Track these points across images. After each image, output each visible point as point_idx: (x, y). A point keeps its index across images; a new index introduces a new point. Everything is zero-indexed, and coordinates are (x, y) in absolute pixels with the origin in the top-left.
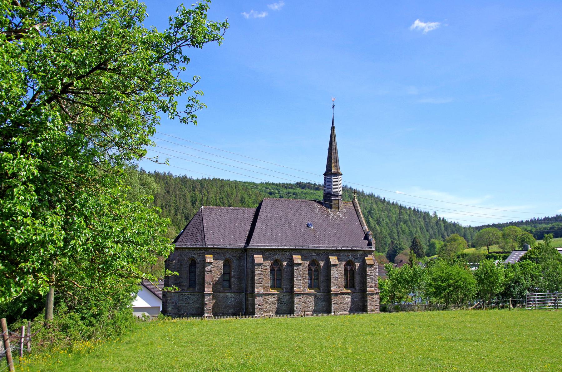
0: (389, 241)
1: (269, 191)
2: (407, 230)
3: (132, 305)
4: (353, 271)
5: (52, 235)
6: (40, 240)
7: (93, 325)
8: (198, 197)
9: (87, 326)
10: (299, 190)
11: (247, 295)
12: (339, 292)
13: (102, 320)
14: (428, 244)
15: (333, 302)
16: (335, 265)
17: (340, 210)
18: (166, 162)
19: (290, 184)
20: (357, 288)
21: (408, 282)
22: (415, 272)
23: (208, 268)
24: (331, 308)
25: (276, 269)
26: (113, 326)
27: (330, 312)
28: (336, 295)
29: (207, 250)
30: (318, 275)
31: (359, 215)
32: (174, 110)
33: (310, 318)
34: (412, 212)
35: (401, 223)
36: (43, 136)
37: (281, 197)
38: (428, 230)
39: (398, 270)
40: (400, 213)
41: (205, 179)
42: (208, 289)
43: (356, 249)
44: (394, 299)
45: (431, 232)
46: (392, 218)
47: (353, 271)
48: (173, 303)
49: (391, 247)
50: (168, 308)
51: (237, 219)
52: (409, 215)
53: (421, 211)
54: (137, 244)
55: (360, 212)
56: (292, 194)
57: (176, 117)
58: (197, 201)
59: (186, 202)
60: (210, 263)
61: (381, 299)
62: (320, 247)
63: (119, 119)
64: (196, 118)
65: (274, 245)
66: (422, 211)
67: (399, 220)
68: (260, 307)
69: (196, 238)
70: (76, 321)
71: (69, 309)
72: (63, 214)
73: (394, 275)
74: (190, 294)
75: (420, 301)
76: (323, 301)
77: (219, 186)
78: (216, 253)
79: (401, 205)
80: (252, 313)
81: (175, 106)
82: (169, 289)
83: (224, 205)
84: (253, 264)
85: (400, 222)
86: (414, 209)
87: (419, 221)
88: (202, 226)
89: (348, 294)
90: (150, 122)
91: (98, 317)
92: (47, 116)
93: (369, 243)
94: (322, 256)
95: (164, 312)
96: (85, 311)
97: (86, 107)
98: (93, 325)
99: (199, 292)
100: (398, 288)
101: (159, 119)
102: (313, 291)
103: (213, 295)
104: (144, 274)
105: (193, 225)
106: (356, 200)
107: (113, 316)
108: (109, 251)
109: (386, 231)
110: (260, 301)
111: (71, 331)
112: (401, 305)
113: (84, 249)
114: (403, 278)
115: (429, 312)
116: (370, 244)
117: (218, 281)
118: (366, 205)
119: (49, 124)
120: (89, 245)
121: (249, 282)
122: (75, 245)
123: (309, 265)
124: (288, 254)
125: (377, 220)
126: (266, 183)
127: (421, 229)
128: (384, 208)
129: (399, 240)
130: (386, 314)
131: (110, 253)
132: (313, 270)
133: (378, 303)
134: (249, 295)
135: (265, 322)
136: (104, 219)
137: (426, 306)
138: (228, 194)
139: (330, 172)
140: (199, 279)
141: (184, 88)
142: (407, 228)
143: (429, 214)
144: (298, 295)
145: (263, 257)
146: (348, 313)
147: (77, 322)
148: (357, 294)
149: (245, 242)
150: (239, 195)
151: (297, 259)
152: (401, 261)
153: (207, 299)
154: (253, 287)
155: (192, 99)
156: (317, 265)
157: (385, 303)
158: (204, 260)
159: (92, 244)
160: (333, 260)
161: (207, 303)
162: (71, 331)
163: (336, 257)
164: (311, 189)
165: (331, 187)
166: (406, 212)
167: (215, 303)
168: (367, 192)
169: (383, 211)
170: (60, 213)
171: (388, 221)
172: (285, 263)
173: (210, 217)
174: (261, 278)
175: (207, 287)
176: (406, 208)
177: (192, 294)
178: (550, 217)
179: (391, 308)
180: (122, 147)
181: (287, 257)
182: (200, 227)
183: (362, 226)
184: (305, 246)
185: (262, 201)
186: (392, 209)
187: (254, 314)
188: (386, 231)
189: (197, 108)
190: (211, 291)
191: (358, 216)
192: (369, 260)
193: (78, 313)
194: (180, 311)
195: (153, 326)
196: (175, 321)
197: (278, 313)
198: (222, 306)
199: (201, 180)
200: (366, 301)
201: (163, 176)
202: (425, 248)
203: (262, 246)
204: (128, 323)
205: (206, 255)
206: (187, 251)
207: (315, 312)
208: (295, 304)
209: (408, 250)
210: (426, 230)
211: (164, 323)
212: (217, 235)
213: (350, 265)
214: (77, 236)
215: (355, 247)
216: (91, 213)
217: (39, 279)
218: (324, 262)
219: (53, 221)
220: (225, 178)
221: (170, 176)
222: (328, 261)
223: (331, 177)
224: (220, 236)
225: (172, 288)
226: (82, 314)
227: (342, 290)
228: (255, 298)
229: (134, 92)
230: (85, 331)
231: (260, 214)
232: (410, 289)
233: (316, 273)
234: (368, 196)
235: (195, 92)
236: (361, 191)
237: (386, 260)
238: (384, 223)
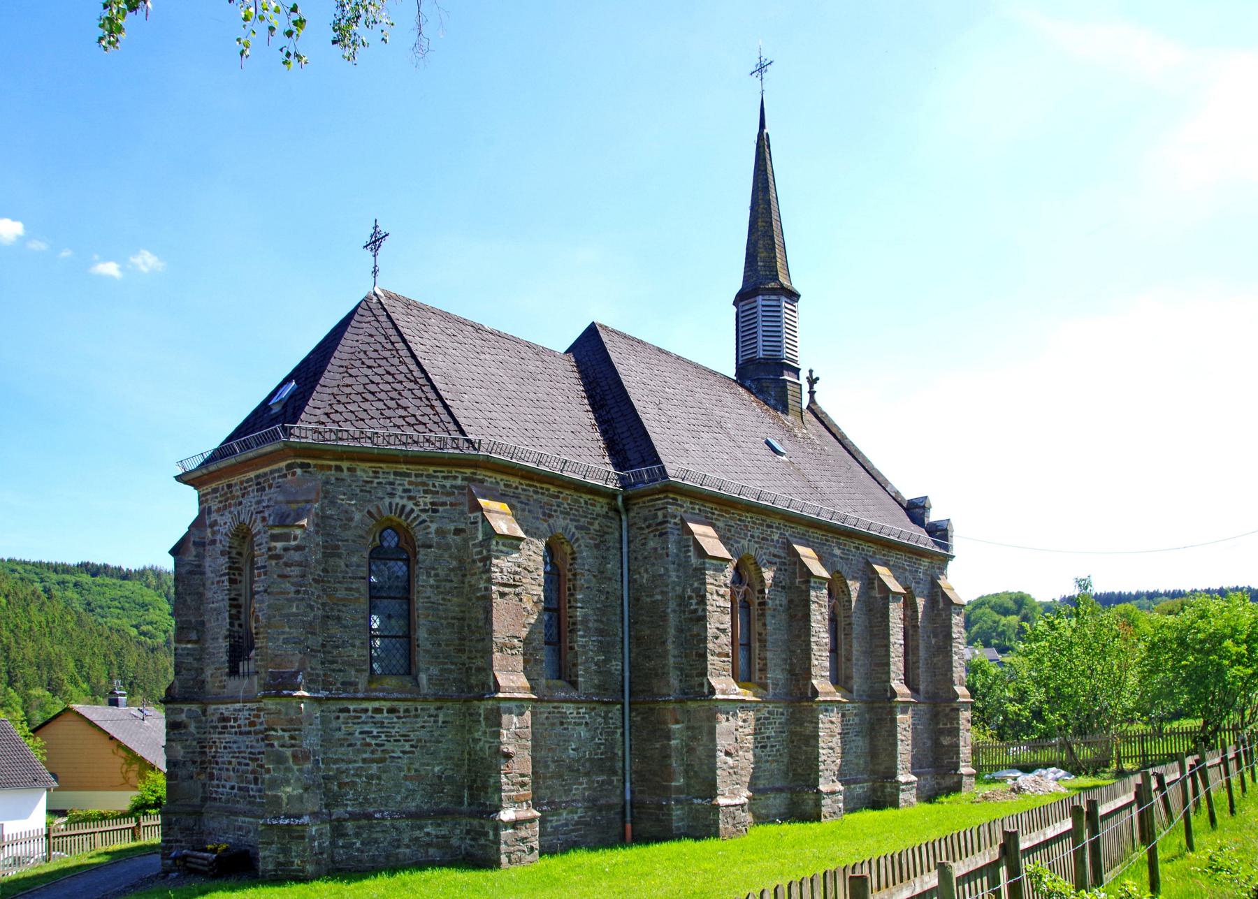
10: (86, 578)
19: (64, 565)
74: (392, 711)
126: (9, 560)
140: (433, 631)
161: (511, 749)
164: (112, 576)
172: (768, 575)
175: (504, 669)
177: (402, 706)
178: (18, 559)
206: (364, 471)
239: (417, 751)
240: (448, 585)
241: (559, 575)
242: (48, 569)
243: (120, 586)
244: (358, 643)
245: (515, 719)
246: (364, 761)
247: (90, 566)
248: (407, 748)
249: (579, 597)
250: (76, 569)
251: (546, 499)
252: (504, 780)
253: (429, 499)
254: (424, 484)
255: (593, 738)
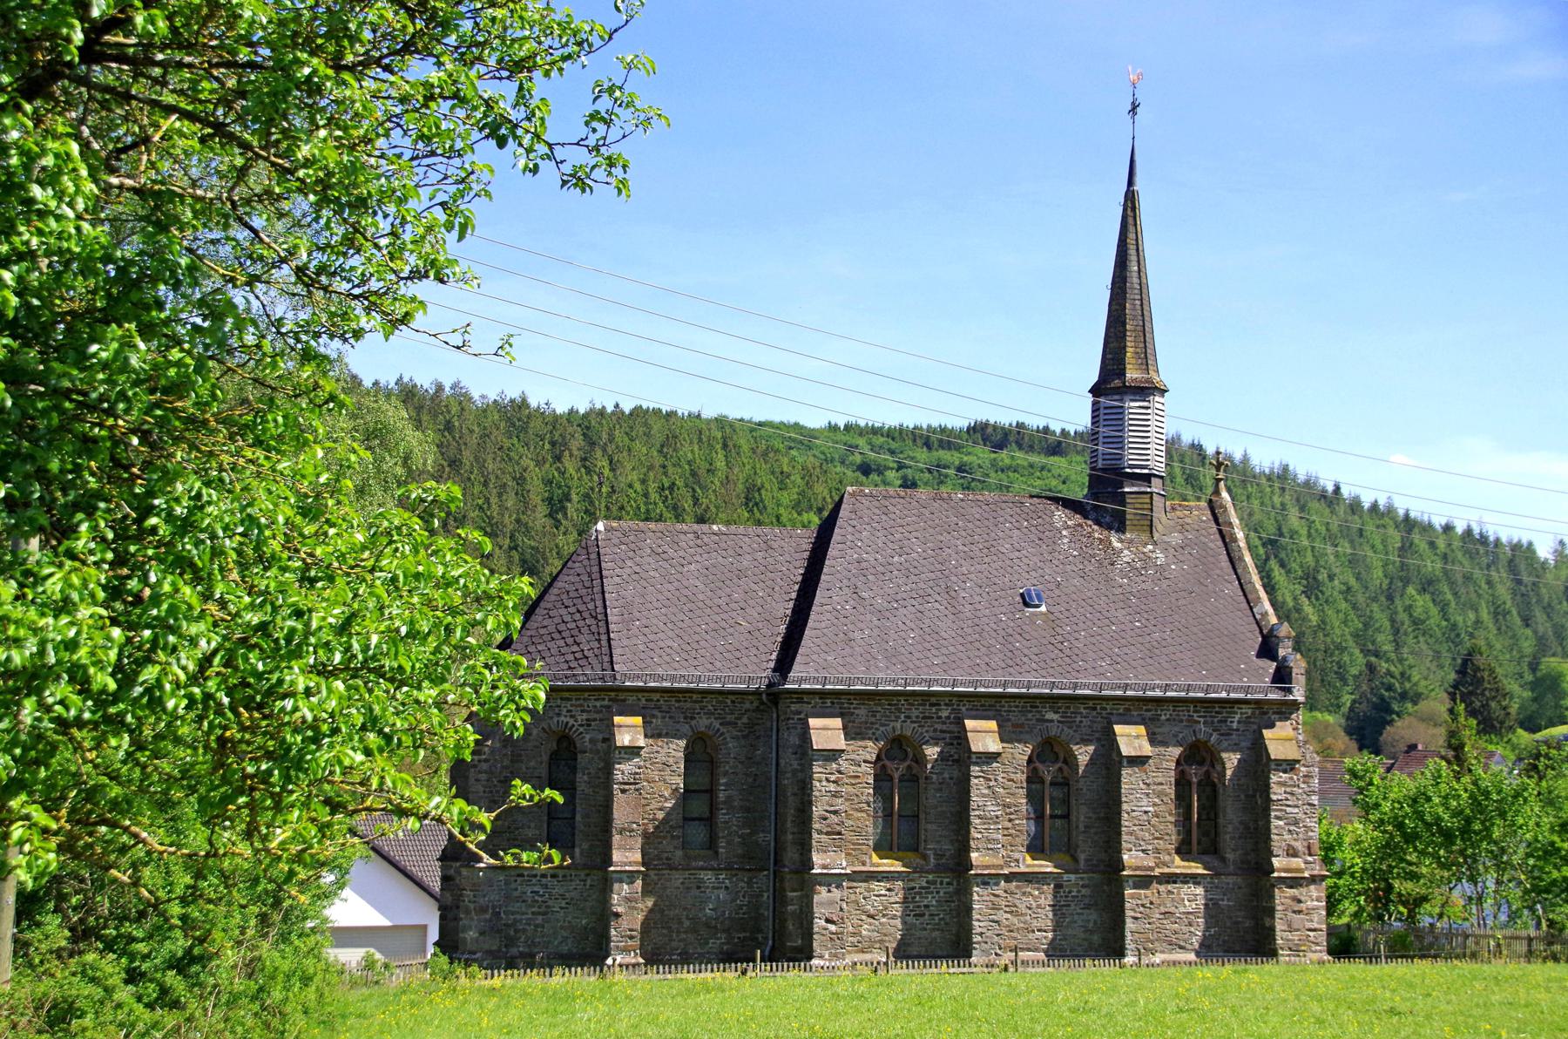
0: (1356, 662)
1: (858, 459)
2: (1435, 619)
3: (326, 920)
4: (1211, 789)
5: (71, 645)
6: (24, 667)
7: (176, 1005)
8: (575, 482)
9: (150, 1006)
10: (980, 455)
11: (782, 880)
12: (1157, 872)
13: (211, 981)
14: (1529, 677)
15: (1129, 913)
16: (1139, 761)
17: (1156, 536)
18: (503, 348)
19: (943, 430)
20: (1230, 856)
21: (1448, 836)
22: (1479, 797)
23: (623, 770)
24: (1123, 937)
25: (896, 776)
26: (256, 1007)
27: (1120, 953)
28: (1144, 882)
29: (622, 696)
30: (1066, 801)
31: (1236, 555)
32: (537, 136)
33: (1042, 975)
34: (1456, 544)
35: (1411, 590)
36: (16, 239)
37: (909, 484)
38: (1527, 622)
39: (1403, 784)
40: (1406, 548)
41: (602, 413)
42: (626, 855)
43: (1224, 695)
44: (1386, 906)
45: (1541, 629)
46: (1368, 568)
47: (1214, 785)
48: (483, 910)
49: (1364, 687)
50: (465, 929)
51: (741, 574)
52: (1445, 557)
53: (1497, 540)
54: (398, 679)
55: (1242, 544)
56: (951, 472)
57: (547, 167)
58: (569, 500)
59: (526, 504)
60: (634, 751)
61: (1332, 906)
62: (1076, 686)
63: (330, 174)
64: (624, 167)
65: (885, 677)
66: (1504, 540)
67: (1402, 577)
68: (833, 928)
69: (575, 648)
70: (106, 990)
71: (74, 940)
72: (103, 561)
73: (1386, 807)
75: (1503, 918)
76: (1088, 907)
77: (658, 438)
78: (658, 708)
79: (1407, 516)
80: (802, 954)
81: (542, 119)
82: (525, 856)
83: (679, 516)
84: (804, 754)
85: (1404, 587)
86: (1468, 532)
87: (1489, 583)
88: (599, 603)
89: (1193, 879)
90: (452, 189)
91: (195, 968)
92: (29, 158)
93: (1278, 670)
94: (1086, 722)
95: (449, 944)
96: (142, 947)
97: (173, 122)
98: (176, 1005)
99: (585, 866)
100: (1402, 860)
101: (486, 177)
102: (1047, 867)
103: (645, 876)
104: (437, 799)
105: (564, 597)
106: (1225, 495)
107: (251, 968)
108: (296, 709)
109: (1345, 622)
110: (831, 903)
111: (84, 1030)
112: (1419, 934)
113: (191, 698)
114: (1428, 818)
115: (1550, 964)
116: (1282, 676)
117: (665, 821)
118: (1257, 517)
119: (36, 191)
120: (212, 685)
121: (789, 825)
122: (159, 684)
123: (1030, 761)
124: (944, 714)
125: (1306, 576)
126: (848, 427)
127: (1498, 613)
128: (1334, 527)
129: (1401, 661)
130: (1356, 969)
131: (298, 714)
132: (1048, 779)
133: (1318, 920)
134: (789, 880)
135: (862, 988)
136: (268, 580)
137: (1530, 940)
138: (694, 474)
139: (1117, 383)
140: (587, 816)
141: (580, 44)
142: (1434, 611)
143: (1534, 552)
144: (986, 880)
145: (845, 728)
146: (1192, 957)
147: (109, 991)
148: (1231, 880)
149: (772, 665)
150: (740, 475)
151: (983, 735)
152: (1413, 747)
153: (620, 895)
154: (805, 848)
155: (611, 91)
156: (1065, 762)
157: (1345, 920)
158: (609, 739)
159: (225, 681)
160: (1131, 738)
161: (620, 910)
162: (84, 1030)
163: (1141, 729)
164: (1031, 448)
165: (1119, 442)
166: (1432, 545)
167: (651, 911)
168: (1264, 458)
169: (1331, 539)
170: (92, 552)
171: (1353, 582)
172: (932, 752)
173: (629, 563)
174: (835, 812)
175: (621, 848)
176: (1430, 525)
178: (862, 423)
179: (1376, 942)
180: (325, 289)
181: (939, 727)
182: (591, 606)
183: (1250, 602)
184: (1013, 684)
185: (842, 498)
186: (1370, 528)
187: (810, 958)
188: (1345, 622)
189: (629, 128)
190: (636, 863)
191: (1234, 561)
192: (1280, 740)
193: (112, 956)
194: (511, 942)
195: (413, 1004)
196: (497, 982)
197: (904, 952)
198: (680, 923)
199: (586, 415)
200: (1271, 912)
201: (432, 399)
202: (1518, 695)
203: (840, 682)
204: (311, 994)
205: (617, 719)
207: (1057, 952)
208: (975, 916)
209: (1438, 704)
210: (1518, 621)
211: (454, 990)
212: (661, 635)
213: (1201, 763)
214: (164, 649)
215: (1223, 688)
216: (217, 552)
217: (12, 822)
218: (1091, 749)
219: (71, 586)
220: (684, 407)
221: (462, 398)
222: (1108, 743)
223: (1121, 400)
224: (670, 643)
225: (536, 855)
226: (132, 957)
227: (1165, 864)
228: (812, 892)
229: (378, 62)
230: (141, 1027)
231: (832, 552)
232: (1459, 865)
233: (1058, 793)
234: (1269, 479)
235: (621, 60)
236: (1238, 456)
237: (1342, 741)
238: (1334, 589)
239: (571, 908)
240: (597, 781)
241: (712, 762)
242: (915, 441)
243: (1042, 469)
244: (532, 825)
245: (625, 887)
246: (533, 913)
247: (990, 430)
248: (563, 905)
249: (723, 781)
250: (965, 436)
251: (688, 705)
252: (613, 932)
253: (585, 716)
254: (581, 705)
255: (734, 900)
